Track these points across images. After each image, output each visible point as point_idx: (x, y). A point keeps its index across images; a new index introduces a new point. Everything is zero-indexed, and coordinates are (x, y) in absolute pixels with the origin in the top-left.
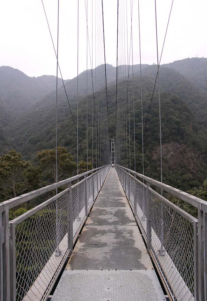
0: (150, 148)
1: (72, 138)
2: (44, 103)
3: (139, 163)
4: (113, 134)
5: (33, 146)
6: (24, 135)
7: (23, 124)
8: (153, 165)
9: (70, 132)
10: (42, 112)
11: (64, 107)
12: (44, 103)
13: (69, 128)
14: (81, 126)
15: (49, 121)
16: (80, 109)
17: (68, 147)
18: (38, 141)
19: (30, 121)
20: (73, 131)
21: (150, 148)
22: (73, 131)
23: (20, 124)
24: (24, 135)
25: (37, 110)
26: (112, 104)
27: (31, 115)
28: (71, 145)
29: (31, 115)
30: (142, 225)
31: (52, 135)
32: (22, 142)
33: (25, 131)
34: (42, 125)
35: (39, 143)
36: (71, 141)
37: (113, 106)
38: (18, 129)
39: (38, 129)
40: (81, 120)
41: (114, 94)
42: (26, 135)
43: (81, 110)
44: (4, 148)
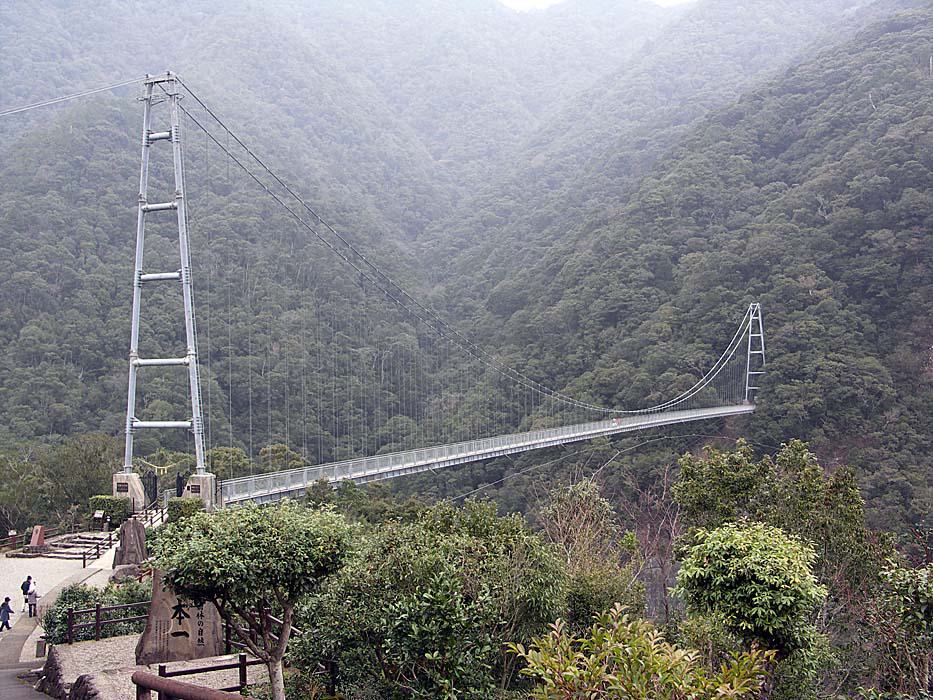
0: (917, 334)
1: (630, 297)
2: (569, 129)
3: (848, 394)
4: (767, 284)
5: (500, 322)
6: (479, 275)
7: (480, 225)
8: (920, 400)
9: (624, 270)
10: (559, 168)
11: (638, 151)
12: (569, 129)
13: (623, 256)
14: (665, 247)
15: (574, 215)
16: (672, 175)
17: (612, 329)
18: (522, 303)
19: (507, 212)
20: (634, 267)
21: (917, 334)
22: (634, 267)
23: (467, 228)
24: (479, 275)
25: (539, 160)
26: (806, 142)
27: (511, 187)
28: (626, 323)
29: (511, 187)
30: (59, 558)
31: (562, 283)
32: (471, 303)
33: (486, 258)
34: (546, 231)
35: (520, 312)
36: (625, 307)
37: (808, 153)
38: (462, 246)
39: (532, 249)
40: (670, 222)
41: (817, 95)
42: (487, 276)
43: (675, 178)
44: (396, 334)
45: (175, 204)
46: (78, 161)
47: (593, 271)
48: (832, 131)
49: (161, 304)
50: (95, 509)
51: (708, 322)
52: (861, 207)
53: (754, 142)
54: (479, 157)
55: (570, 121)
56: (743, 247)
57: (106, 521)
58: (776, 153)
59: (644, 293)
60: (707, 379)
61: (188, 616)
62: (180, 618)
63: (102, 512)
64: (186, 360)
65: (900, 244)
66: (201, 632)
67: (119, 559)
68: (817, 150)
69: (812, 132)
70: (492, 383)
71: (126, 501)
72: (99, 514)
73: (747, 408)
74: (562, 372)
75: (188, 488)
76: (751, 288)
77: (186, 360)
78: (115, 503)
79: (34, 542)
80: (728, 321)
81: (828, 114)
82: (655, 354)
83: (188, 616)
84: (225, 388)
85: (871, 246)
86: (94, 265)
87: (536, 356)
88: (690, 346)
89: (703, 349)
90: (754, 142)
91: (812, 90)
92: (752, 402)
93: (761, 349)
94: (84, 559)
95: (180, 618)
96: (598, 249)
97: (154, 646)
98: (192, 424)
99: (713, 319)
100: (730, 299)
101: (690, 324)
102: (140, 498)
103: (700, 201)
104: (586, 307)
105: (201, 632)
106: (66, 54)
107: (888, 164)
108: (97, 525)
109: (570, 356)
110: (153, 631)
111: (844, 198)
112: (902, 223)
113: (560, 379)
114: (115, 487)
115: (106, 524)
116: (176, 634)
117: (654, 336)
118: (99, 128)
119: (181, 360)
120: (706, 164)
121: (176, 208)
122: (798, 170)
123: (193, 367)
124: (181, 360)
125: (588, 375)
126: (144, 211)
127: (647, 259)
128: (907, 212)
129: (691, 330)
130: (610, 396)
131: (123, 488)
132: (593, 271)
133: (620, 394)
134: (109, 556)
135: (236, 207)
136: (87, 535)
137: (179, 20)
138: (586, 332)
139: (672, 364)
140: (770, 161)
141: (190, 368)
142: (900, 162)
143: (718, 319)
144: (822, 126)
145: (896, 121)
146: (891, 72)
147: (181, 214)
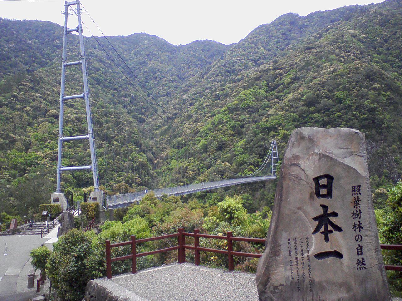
28: (225, 150)
41: (287, 70)
45: (81, 61)
46: (15, 95)
47: (212, 132)
48: (293, 82)
49: (49, 147)
50: (42, 210)
51: (257, 147)
52: (307, 106)
53: (266, 86)
54: (164, 96)
55: (196, 83)
56: (267, 121)
57: (48, 216)
58: (273, 90)
59: (231, 139)
60: (266, 162)
61: (339, 229)
62: (326, 234)
63: (46, 212)
64: (88, 136)
65: (322, 118)
66: (360, 250)
67: (60, 232)
68: (288, 88)
69: (286, 83)
70: (176, 173)
71: (58, 207)
72: (44, 213)
73: (273, 177)
74: (202, 168)
75: (90, 198)
76: (271, 135)
77: (88, 136)
78: (52, 207)
79: (12, 227)
80: (264, 146)
81: (291, 76)
82: (240, 158)
83: (339, 229)
84: (75, 178)
85: (312, 119)
86: (22, 133)
87: (192, 163)
88: (251, 156)
89: (256, 157)
90: (266, 86)
91: (284, 68)
92: (274, 175)
93: (277, 156)
94: (41, 234)
95: (326, 234)
96: (213, 124)
97: (289, 273)
98: (91, 167)
99: (258, 146)
100: (264, 139)
101: (250, 149)
102: (65, 205)
103: (249, 107)
104: (210, 145)
105: (360, 250)
106: (9, 58)
107: (315, 91)
108: (44, 218)
109: (205, 162)
110: (284, 253)
111: (302, 103)
112: (322, 111)
113: (201, 170)
114: (52, 200)
115: (48, 218)
116: (320, 256)
117: (236, 153)
118: (23, 83)
119: (85, 136)
120: (250, 94)
121: (81, 64)
122: (282, 96)
123: (91, 140)
124: (85, 136)
125: (212, 168)
126: (65, 66)
127: (231, 127)
128: (324, 107)
129: (251, 150)
130: (222, 175)
131: (56, 200)
132: (212, 132)
133: (226, 174)
134: (55, 231)
135: (77, 112)
136: (39, 223)
137: (52, 46)
138: (211, 153)
139: (245, 163)
140: (272, 92)
141: (90, 140)
142: (320, 91)
143: (261, 146)
144: (289, 80)
145: (315, 78)
146: (311, 62)
147: (84, 66)
